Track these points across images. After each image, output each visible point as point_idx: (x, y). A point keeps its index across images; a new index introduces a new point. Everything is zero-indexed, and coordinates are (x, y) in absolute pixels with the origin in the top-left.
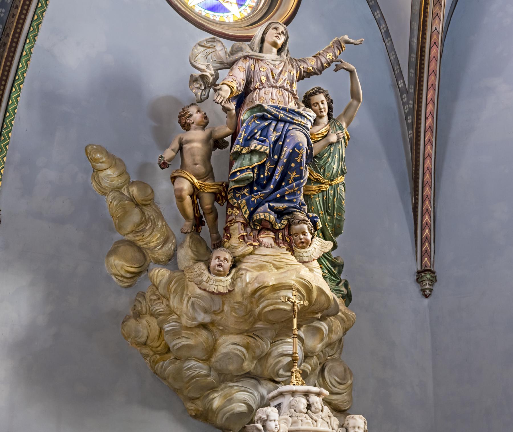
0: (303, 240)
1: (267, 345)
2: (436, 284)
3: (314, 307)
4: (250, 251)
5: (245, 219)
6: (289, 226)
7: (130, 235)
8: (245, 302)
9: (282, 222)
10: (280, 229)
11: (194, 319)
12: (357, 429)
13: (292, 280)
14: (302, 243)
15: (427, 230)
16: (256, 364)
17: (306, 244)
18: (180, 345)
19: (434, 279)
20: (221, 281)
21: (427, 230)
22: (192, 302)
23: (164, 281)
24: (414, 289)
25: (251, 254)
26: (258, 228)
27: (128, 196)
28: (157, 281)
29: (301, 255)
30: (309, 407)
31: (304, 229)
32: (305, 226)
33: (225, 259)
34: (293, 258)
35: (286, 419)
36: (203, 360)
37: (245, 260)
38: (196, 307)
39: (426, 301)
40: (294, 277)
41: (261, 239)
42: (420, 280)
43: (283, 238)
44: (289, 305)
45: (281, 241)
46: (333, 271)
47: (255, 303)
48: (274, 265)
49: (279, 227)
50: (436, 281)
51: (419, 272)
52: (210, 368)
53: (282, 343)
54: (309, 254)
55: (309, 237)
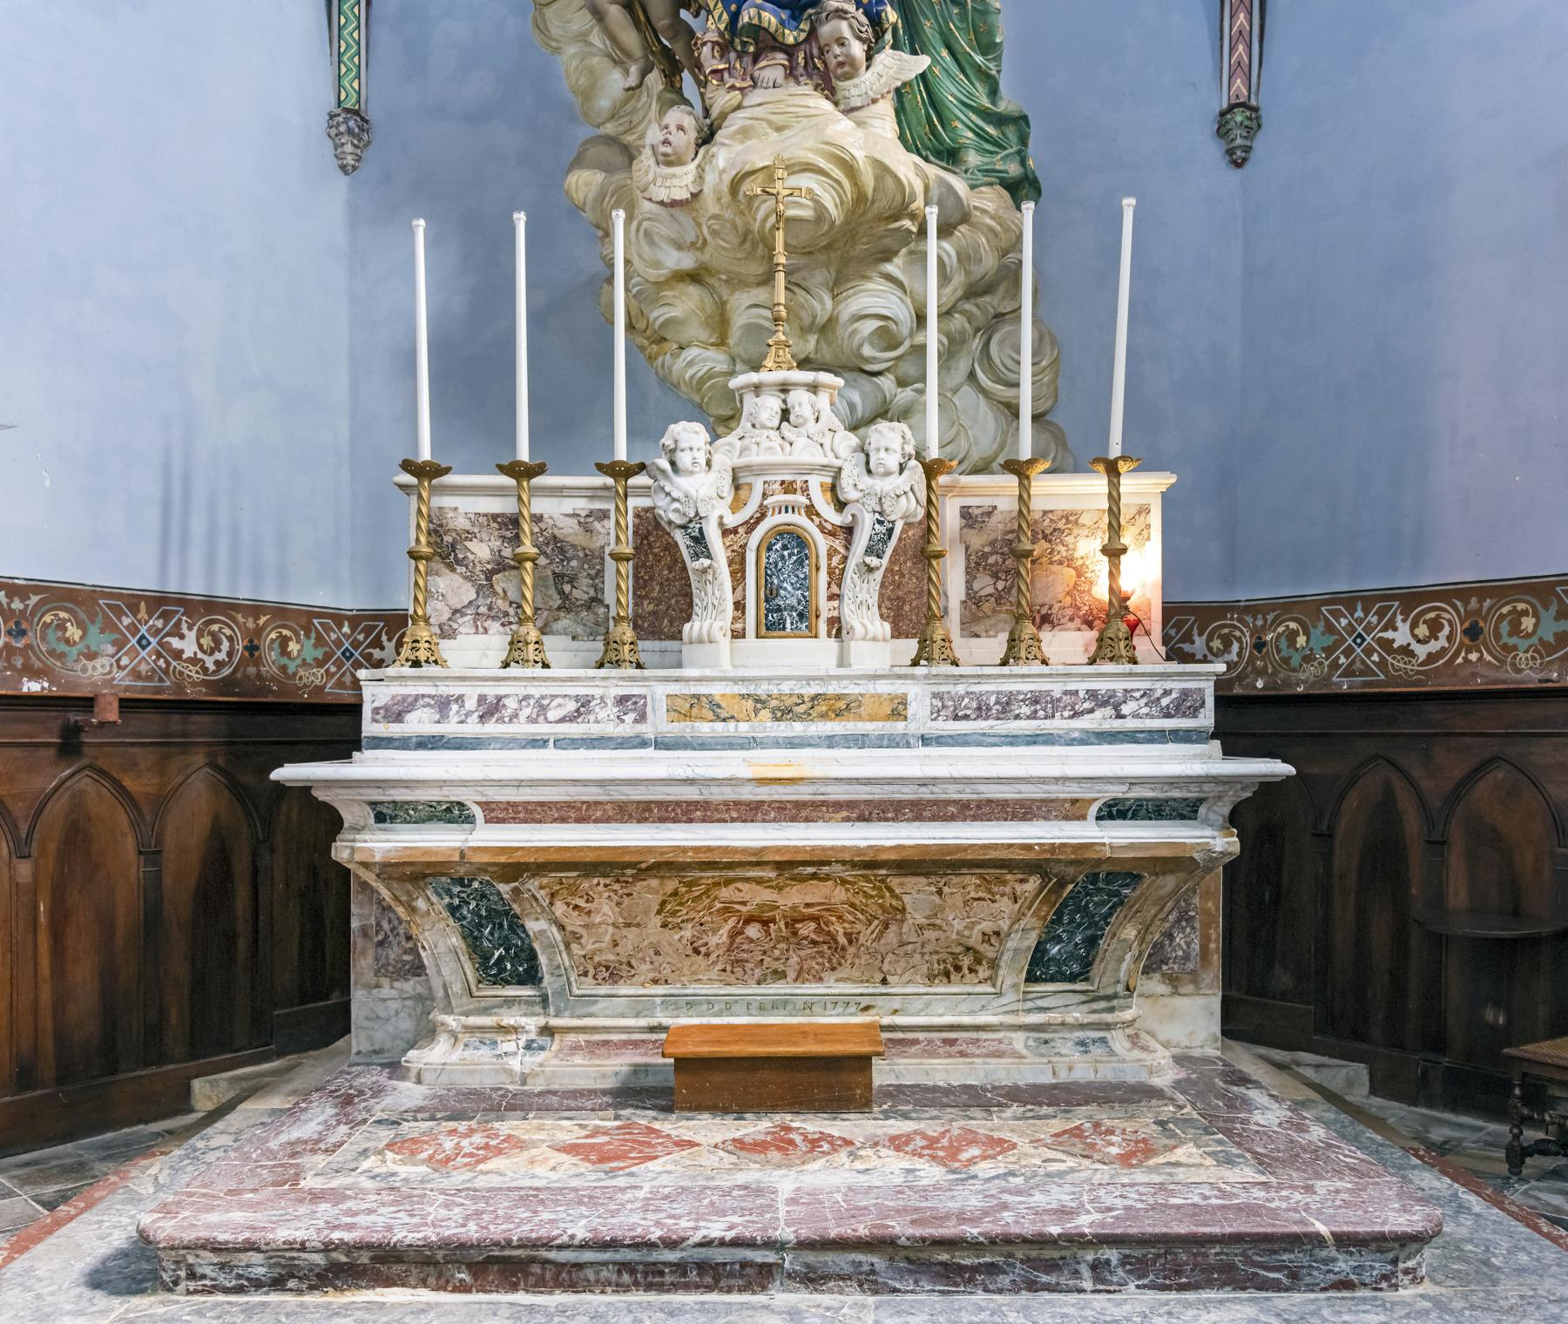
0: (840, 59)
1: (822, 302)
2: (1260, 134)
3: (876, 205)
4: (735, 102)
5: (721, 34)
6: (812, 33)
7: (608, 125)
8: (728, 214)
9: (802, 26)
10: (797, 45)
11: (657, 265)
12: (883, 451)
13: (802, 147)
14: (841, 64)
15: (1242, 15)
16: (818, 342)
17: (849, 69)
18: (662, 319)
19: (1254, 124)
20: (674, 176)
21: (1242, 15)
22: (646, 231)
23: (591, 196)
24: (1212, 151)
25: (739, 107)
26: (752, 49)
27: (602, 46)
28: (579, 196)
29: (847, 94)
30: (785, 415)
31: (840, 31)
32: (844, 25)
33: (680, 128)
34: (827, 105)
35: (730, 444)
36: (712, 344)
37: (726, 123)
38: (657, 239)
39: (1236, 175)
40: (810, 143)
41: (756, 74)
42: (1223, 130)
43: (806, 63)
44: (807, 206)
45: (801, 70)
46: (987, 133)
47: (746, 212)
48: (769, 123)
49: (795, 39)
50: (1259, 126)
51: (1223, 114)
52: (733, 359)
53: (855, 294)
54: (863, 89)
55: (858, 50)
